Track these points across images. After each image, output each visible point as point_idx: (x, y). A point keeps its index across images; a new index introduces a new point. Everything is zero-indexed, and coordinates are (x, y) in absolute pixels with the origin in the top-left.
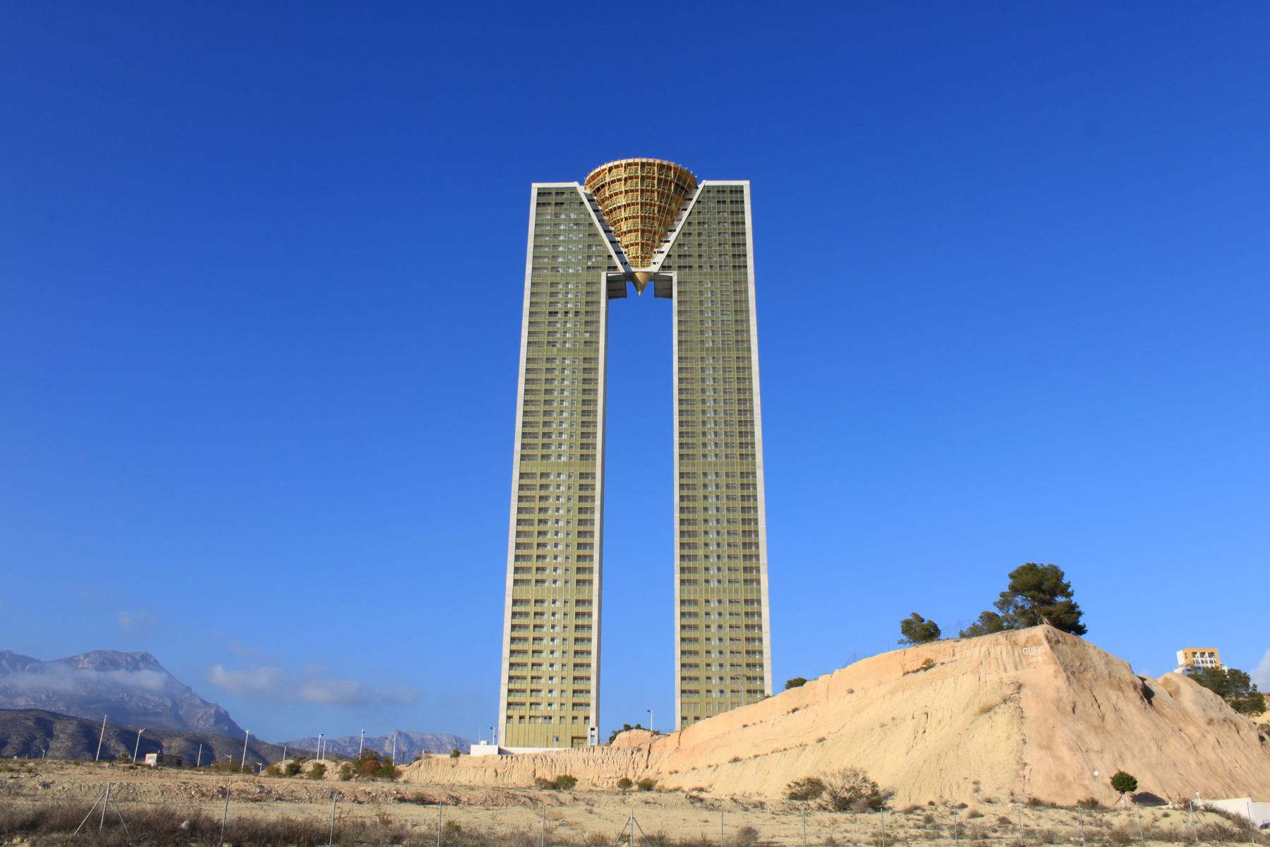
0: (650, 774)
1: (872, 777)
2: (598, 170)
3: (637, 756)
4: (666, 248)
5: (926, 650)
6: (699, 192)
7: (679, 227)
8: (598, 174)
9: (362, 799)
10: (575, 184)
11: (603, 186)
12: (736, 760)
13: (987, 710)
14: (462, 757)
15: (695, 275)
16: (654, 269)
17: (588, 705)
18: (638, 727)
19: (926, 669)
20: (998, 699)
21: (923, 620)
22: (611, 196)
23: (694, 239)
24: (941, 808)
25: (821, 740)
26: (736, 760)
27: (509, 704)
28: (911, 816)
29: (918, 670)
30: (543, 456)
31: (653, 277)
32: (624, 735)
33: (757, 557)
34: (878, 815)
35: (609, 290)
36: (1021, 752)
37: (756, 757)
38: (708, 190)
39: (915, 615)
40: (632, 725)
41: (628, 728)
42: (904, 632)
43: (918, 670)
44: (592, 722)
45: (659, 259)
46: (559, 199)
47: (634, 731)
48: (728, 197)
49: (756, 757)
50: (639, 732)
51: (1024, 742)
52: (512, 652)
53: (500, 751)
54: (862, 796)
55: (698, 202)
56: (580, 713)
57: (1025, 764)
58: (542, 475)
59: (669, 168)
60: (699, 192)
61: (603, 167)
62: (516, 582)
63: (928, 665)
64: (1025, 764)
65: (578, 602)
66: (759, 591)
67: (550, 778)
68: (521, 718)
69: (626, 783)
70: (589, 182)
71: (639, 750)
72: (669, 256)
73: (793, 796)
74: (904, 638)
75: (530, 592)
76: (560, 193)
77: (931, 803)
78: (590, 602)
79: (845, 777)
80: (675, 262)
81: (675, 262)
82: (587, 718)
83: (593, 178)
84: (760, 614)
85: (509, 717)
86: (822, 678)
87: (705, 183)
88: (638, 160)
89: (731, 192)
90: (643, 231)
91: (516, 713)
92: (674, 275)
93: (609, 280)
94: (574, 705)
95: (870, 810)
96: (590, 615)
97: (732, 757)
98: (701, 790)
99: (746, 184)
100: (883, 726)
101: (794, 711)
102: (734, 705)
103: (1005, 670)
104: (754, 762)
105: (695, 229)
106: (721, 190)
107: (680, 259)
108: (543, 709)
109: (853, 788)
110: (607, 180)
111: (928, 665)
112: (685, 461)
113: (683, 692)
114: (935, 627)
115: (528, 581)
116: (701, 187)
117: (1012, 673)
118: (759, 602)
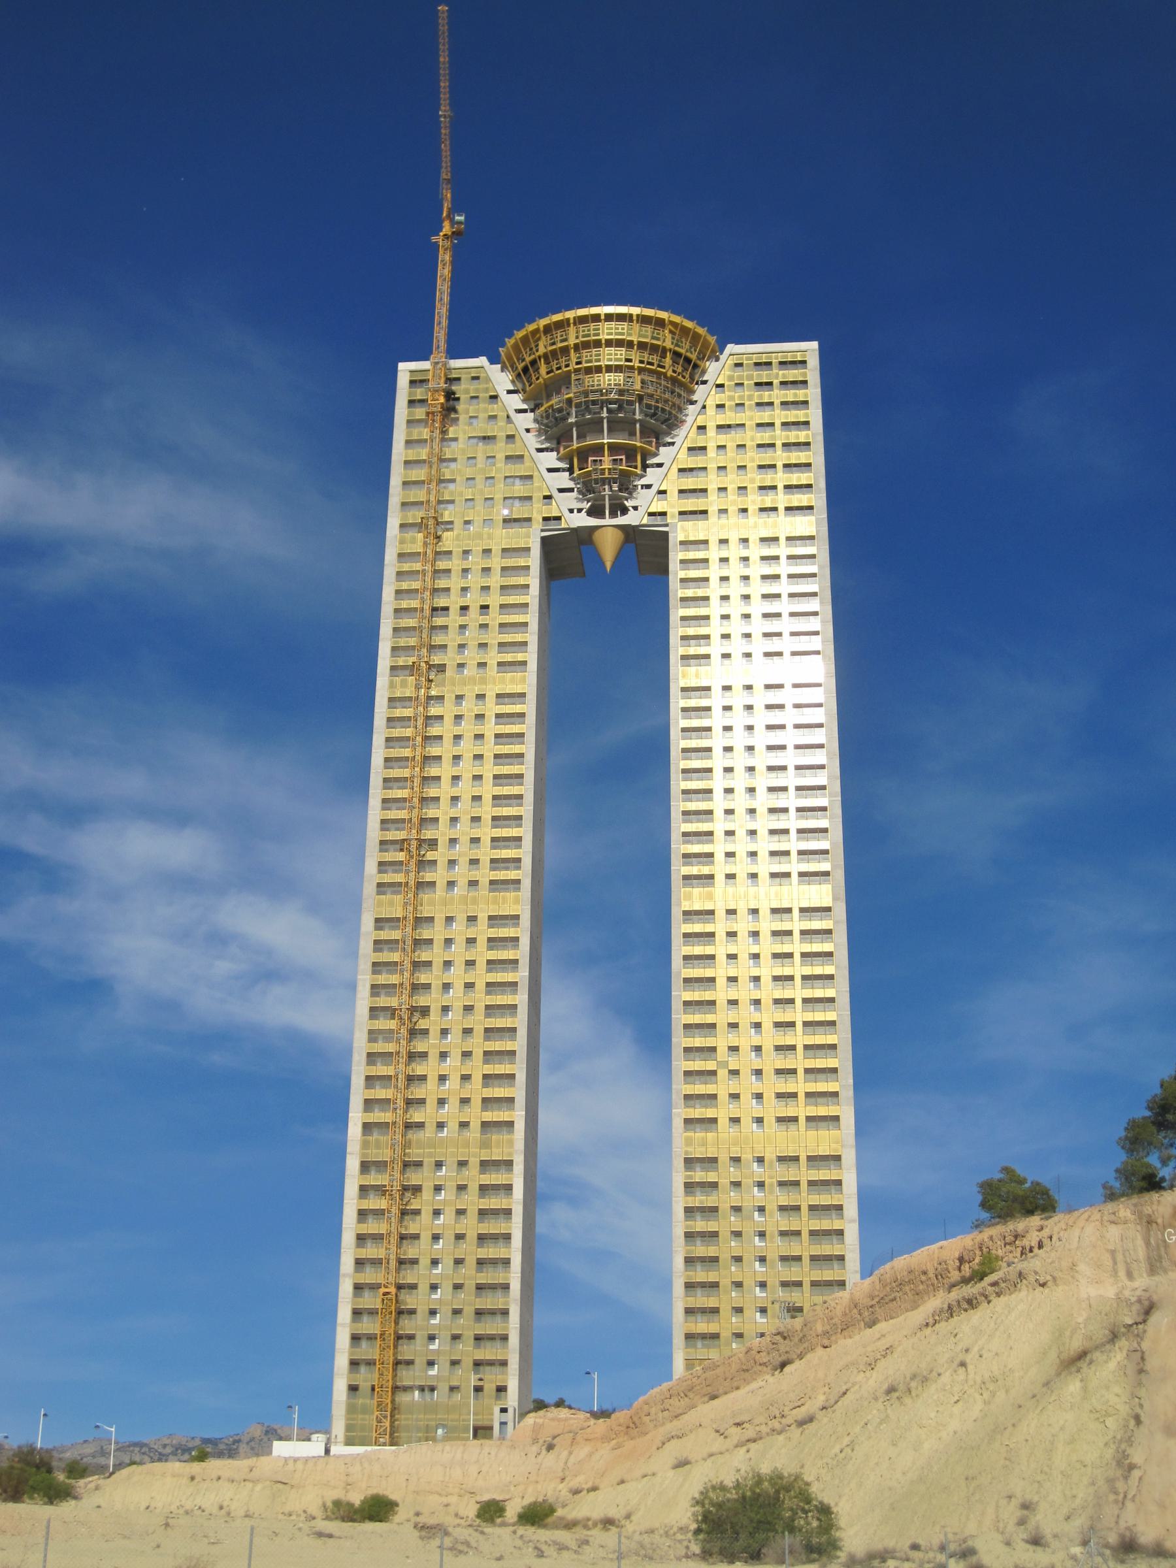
2: (557, 317)
8: (525, 340)
10: (482, 361)
13: (1077, 1360)
17: (504, 1363)
18: (560, 1404)
20: (1101, 1334)
21: (1022, 1182)
36: (1130, 1441)
39: (1006, 1170)
40: (550, 1399)
42: (984, 1205)
47: (554, 1412)
50: (563, 1413)
51: (1138, 1419)
52: (359, 1263)
56: (491, 1379)
57: (1132, 1467)
64: (1132, 1467)
65: (485, 1165)
71: (550, 1447)
74: (985, 1215)
82: (501, 1389)
85: (353, 1389)
103: (1130, 1275)
110: (572, 341)
113: (689, 1337)
114: (1045, 1193)
117: (1142, 1281)
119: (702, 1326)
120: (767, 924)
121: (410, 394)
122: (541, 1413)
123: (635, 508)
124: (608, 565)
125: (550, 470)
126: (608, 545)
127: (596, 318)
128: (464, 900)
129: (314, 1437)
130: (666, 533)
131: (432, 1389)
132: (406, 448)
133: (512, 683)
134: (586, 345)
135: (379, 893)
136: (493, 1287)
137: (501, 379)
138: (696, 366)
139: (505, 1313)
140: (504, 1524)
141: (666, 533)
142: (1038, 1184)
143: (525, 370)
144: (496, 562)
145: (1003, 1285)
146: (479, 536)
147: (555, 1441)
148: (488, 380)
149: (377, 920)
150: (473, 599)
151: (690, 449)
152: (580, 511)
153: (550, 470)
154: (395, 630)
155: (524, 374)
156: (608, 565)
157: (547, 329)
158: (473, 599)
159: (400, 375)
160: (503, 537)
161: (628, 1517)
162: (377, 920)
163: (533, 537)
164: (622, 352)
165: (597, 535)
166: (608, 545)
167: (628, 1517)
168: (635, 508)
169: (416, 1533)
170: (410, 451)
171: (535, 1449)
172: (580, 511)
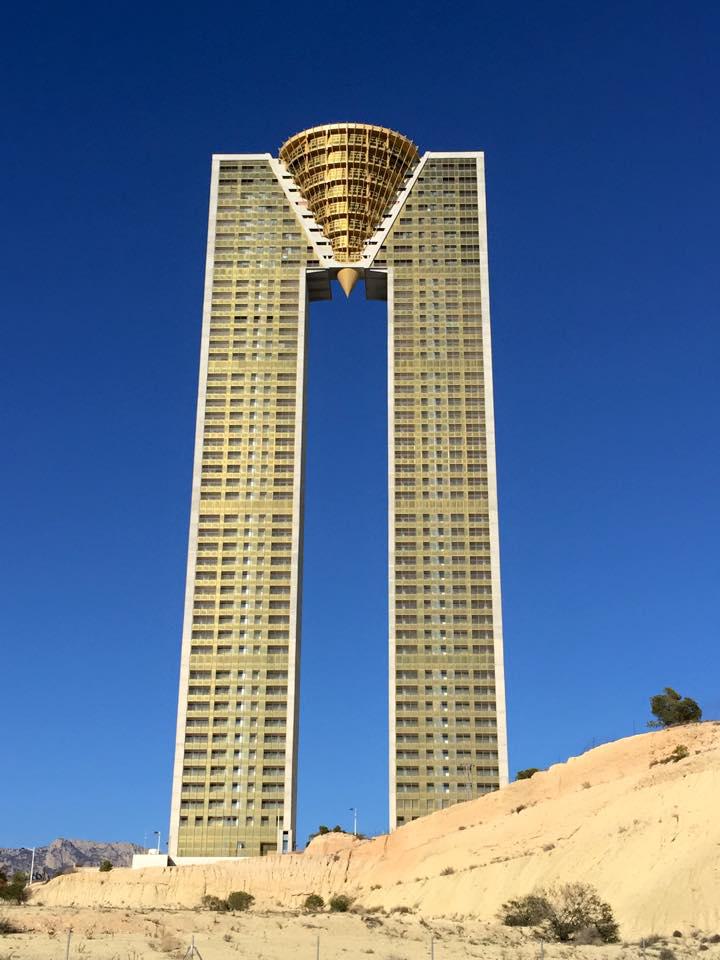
0: (347, 890)
1: (604, 898)
2: (294, 139)
3: (335, 866)
4: (379, 237)
5: (679, 734)
6: (420, 166)
7: (395, 210)
8: (296, 144)
9: (476, 942)
10: (267, 156)
11: (302, 159)
12: (448, 872)
14: (116, 871)
15: (415, 273)
16: (365, 264)
17: (281, 802)
18: (337, 830)
19: (677, 759)
22: (312, 172)
23: (415, 226)
24: (690, 941)
25: (550, 848)
26: (448, 872)
27: (184, 802)
28: (648, 950)
29: (668, 760)
30: (228, 494)
31: (363, 275)
32: (319, 840)
33: (490, 618)
34: (609, 947)
35: (310, 290)
37: (472, 868)
38: (432, 164)
39: (669, 691)
41: (324, 831)
43: (668, 760)
44: (287, 825)
45: (371, 251)
46: (249, 175)
47: (333, 835)
48: (457, 173)
49: (472, 868)
53: (170, 863)
54: (589, 921)
55: (420, 179)
56: (272, 812)
58: (227, 517)
59: (383, 137)
60: (420, 166)
61: (301, 135)
62: (194, 649)
63: (680, 754)
66: (492, 660)
67: (223, 896)
68: (199, 819)
69: (314, 902)
70: (285, 155)
71: (336, 859)
72: (383, 248)
73: (511, 921)
74: (655, 719)
75: (211, 662)
76: (247, 168)
77: (677, 934)
78: (285, 674)
79: (568, 895)
80: (391, 255)
81: (391, 255)
83: (290, 149)
84: (493, 689)
85: (183, 819)
86: (553, 768)
87: (429, 155)
88: (368, 127)
89: (461, 166)
90: (351, 233)
91: (192, 812)
92: (391, 272)
93: (309, 277)
94: (264, 802)
95: (599, 940)
96: (284, 689)
97: (444, 868)
98: (404, 910)
99: (479, 156)
100: (622, 831)
101: (519, 810)
102: (445, 803)
104: (469, 875)
105: (415, 213)
106: (448, 164)
107: (400, 249)
108: (224, 809)
109: (578, 911)
110: (307, 151)
111: (680, 754)
112: (403, 500)
114: (695, 707)
115: (209, 648)
116: (423, 160)
118: (492, 674)
119: (408, 778)
120: (448, 524)
121: (220, 176)
122: (324, 835)
123: (366, 257)
124: (347, 293)
125: (312, 230)
126: (346, 280)
127: (319, 134)
128: (257, 504)
129: (151, 851)
130: (386, 274)
131: (235, 819)
132: (218, 211)
133: (216, 367)
134: (314, 154)
135: (202, 499)
136: (274, 752)
137: (279, 168)
138: (405, 166)
139: (282, 769)
140: (323, 912)
141: (386, 274)
142: (689, 699)
143: (296, 163)
144: (277, 289)
145: (694, 765)
146: (266, 271)
147: (339, 855)
148: (270, 169)
149: (201, 516)
150: (262, 312)
151: (401, 220)
152: (330, 257)
153: (312, 230)
154: (212, 330)
155: (294, 166)
156: (347, 293)
157: (311, 137)
158: (262, 312)
159: (213, 163)
160: (280, 273)
161: (416, 906)
162: (201, 516)
163: (302, 274)
164: (338, 154)
165: (341, 274)
166: (346, 280)
167: (416, 906)
168: (366, 257)
169: (365, 925)
170: (221, 214)
171: (325, 861)
172: (330, 257)
